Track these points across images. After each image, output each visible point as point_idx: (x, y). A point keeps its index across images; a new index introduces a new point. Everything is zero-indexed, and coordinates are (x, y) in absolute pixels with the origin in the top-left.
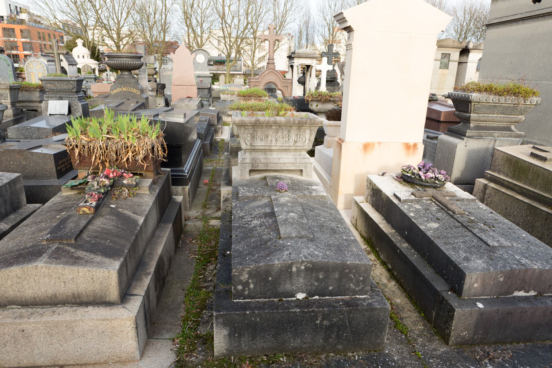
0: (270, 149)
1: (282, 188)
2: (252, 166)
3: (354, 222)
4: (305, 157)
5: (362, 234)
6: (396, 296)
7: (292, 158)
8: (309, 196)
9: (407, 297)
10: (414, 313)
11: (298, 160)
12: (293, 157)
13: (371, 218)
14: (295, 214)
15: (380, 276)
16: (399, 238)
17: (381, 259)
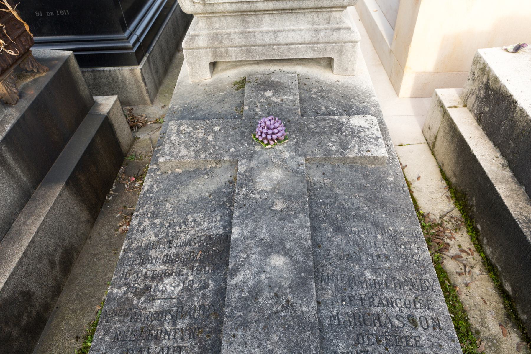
0: (253, 8)
1: (269, 137)
2: (215, 54)
4: (340, 26)
7: (309, 30)
8: (340, 159)
11: (322, 34)
12: (309, 26)
13: (474, 157)
14: (287, 260)
15: (483, 307)
17: (485, 253)
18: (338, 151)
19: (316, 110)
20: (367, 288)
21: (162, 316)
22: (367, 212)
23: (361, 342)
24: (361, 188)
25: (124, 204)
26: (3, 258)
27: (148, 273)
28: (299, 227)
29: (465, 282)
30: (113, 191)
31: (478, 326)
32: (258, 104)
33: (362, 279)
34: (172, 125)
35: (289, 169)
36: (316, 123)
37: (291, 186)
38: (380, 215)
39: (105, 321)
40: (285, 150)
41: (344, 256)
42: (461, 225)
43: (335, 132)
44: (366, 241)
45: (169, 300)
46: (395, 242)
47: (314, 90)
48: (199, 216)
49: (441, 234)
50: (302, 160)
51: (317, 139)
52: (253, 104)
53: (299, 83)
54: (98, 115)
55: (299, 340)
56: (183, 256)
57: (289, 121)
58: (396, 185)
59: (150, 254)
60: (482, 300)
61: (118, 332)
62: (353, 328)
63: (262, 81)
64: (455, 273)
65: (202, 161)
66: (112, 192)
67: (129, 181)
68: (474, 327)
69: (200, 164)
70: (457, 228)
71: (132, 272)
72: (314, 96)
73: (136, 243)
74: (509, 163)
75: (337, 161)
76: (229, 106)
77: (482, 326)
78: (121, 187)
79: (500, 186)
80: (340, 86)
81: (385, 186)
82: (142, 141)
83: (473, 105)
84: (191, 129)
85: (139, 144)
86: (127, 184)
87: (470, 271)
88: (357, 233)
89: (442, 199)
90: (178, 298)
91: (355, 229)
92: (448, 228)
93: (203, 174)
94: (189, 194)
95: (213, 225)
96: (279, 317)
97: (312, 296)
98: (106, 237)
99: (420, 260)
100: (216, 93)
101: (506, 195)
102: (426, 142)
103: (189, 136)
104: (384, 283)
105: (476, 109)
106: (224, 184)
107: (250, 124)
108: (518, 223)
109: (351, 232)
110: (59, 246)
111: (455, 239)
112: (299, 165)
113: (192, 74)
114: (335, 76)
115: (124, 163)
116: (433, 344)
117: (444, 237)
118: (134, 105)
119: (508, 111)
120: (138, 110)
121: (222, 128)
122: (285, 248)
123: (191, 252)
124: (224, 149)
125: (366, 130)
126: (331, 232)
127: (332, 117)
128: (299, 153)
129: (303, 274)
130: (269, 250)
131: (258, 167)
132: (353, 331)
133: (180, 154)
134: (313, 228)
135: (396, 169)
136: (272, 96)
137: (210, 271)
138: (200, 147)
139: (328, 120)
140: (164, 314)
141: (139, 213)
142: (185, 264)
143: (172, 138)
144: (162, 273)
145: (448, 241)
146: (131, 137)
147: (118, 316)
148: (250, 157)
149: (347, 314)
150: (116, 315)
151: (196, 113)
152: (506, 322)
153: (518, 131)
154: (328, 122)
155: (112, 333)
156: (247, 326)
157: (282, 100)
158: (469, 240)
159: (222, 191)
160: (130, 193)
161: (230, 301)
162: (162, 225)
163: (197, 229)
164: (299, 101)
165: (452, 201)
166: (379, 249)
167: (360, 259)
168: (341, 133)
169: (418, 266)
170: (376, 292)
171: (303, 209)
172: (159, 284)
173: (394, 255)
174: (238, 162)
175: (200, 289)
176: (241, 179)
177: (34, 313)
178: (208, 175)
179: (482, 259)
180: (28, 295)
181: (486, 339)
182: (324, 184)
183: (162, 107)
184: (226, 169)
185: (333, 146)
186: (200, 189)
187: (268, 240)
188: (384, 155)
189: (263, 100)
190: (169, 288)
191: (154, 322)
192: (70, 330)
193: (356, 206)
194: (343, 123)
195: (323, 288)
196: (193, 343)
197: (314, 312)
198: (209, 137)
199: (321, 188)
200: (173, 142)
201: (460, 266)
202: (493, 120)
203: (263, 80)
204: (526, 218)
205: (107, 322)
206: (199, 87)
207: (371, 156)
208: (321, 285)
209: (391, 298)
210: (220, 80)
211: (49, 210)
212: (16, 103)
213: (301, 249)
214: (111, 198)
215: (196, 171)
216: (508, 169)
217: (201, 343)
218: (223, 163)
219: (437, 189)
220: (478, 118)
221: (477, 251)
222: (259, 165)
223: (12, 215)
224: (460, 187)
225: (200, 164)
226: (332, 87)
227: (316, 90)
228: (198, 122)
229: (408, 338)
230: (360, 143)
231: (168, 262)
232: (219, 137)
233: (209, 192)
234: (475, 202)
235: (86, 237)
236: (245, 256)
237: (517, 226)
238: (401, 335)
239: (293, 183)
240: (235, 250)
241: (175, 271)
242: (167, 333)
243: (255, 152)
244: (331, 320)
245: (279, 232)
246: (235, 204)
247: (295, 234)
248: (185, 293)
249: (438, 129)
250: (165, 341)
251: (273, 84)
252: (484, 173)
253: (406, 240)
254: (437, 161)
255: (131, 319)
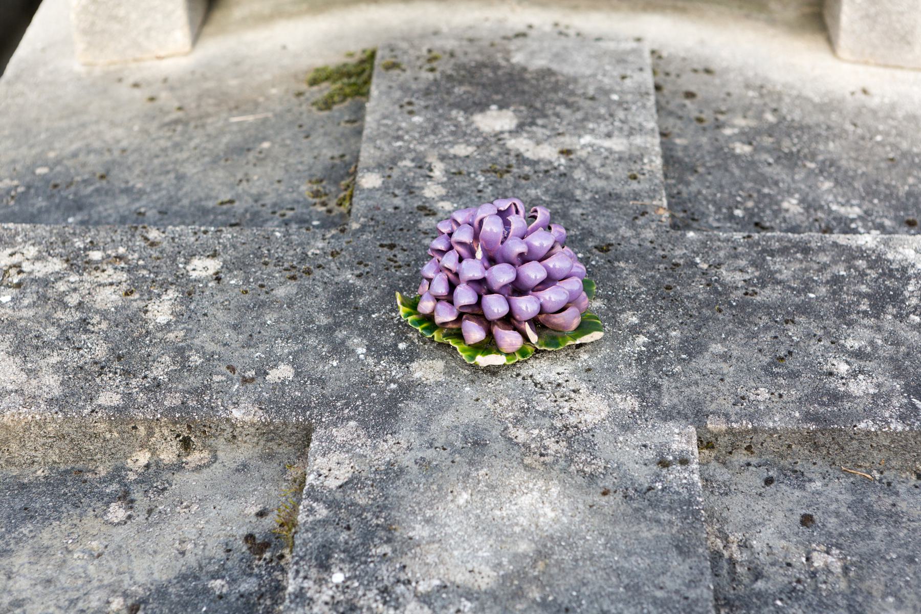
1: (496, 306)
18: (888, 400)
32: (438, 171)
35: (608, 483)
36: (753, 264)
37: (618, 572)
43: (863, 307)
47: (740, 122)
51: (768, 337)
52: (408, 163)
53: (658, 88)
63: (459, 67)
65: (102, 427)
72: (741, 149)
75: (885, 454)
76: (279, 174)
80: (874, 112)
84: (56, 265)
93: (101, 496)
100: (208, 115)
103: (44, 298)
106: (221, 554)
107: (390, 254)
112: (664, 464)
113: (93, 24)
114: (846, 67)
121: (228, 267)
124: (232, 369)
128: (666, 401)
131: (422, 463)
136: (514, 133)
139: (821, 249)
151: (92, 205)
154: (824, 258)
157: (566, 152)
159: (206, 591)
164: (658, 162)
176: (325, 522)
182: (813, 575)
184: (239, 477)
186: (76, 577)
189: (461, 150)
194: (904, 270)
203: (464, 60)
206: (124, 91)
210: (237, 64)
215: (64, 483)
218: (220, 443)
222: (429, 454)
226: (834, 116)
227: (752, 123)
228: (103, 235)
232: (212, 311)
233: (125, 595)
239: (630, 553)
243: (408, 390)
251: (523, 80)
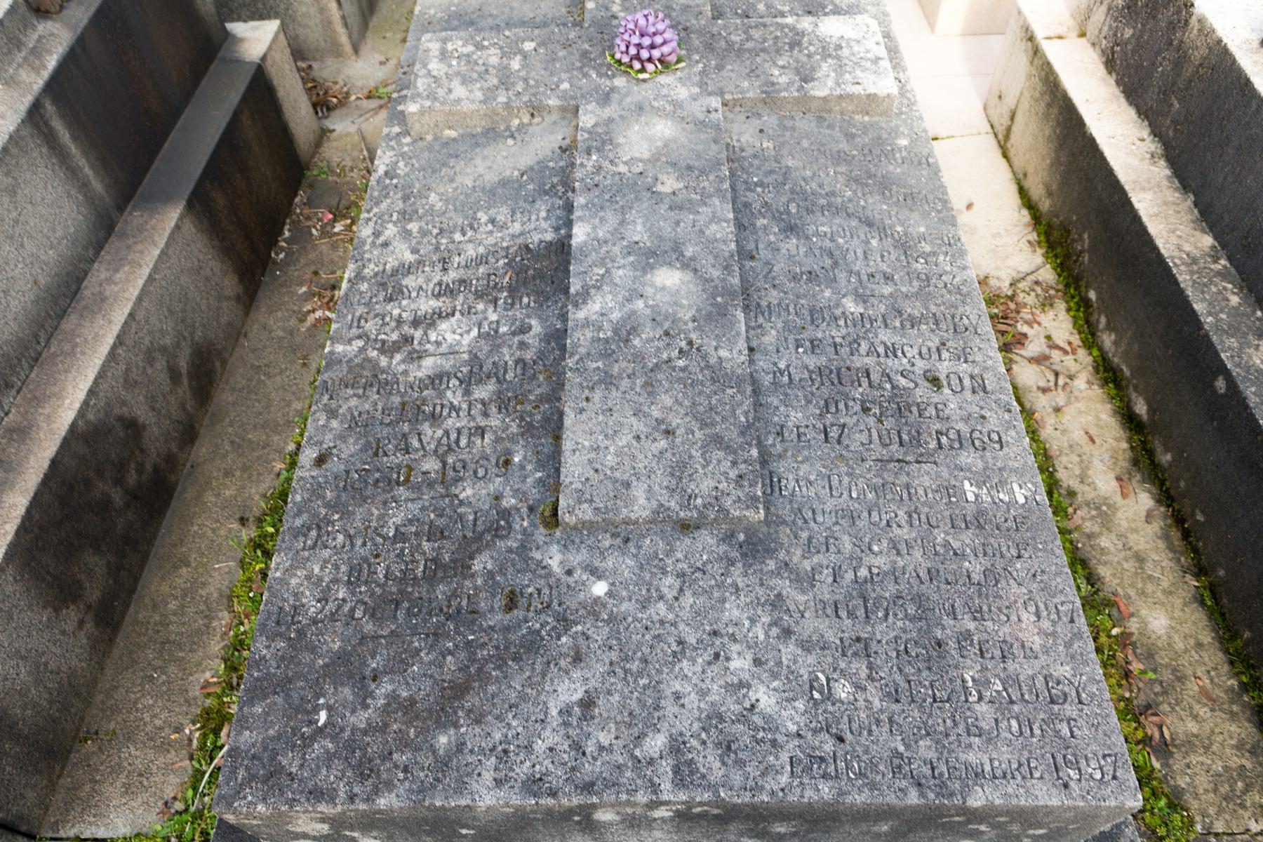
1: (645, 54)
3: (1002, 122)
5: (1026, 184)
6: (1150, 588)
8: (797, 101)
9: (1202, 603)
10: (1233, 716)
13: (1092, 142)
14: (689, 276)
15: (1087, 448)
16: (1235, 300)
17: (1100, 349)
19: (744, 11)
20: (846, 326)
21: (441, 381)
22: (850, 200)
23: (833, 410)
24: (839, 158)
25: (313, 268)
26: (76, 345)
27: (404, 315)
28: (711, 222)
29: (1054, 404)
30: (285, 240)
31: (1074, 484)
33: (838, 312)
34: (430, 41)
36: (744, 33)
38: (876, 206)
39: (326, 397)
40: (679, 85)
41: (802, 273)
42: (1055, 297)
44: (847, 250)
45: (452, 356)
46: (905, 253)
48: (502, 214)
49: (1010, 315)
50: (715, 102)
54: (239, 62)
55: (714, 402)
56: (474, 282)
57: (685, 29)
58: (912, 154)
59: (404, 283)
60: (1086, 436)
61: (356, 414)
62: (818, 389)
64: (1035, 389)
65: (501, 110)
66: (284, 244)
67: (320, 220)
68: (1065, 485)
69: (496, 118)
70: (1047, 303)
71: (372, 315)
73: (372, 266)
74: (1166, 149)
77: (1082, 482)
78: (302, 235)
79: (1142, 195)
81: (889, 155)
82: (341, 136)
83: (1100, 30)
84: (470, 48)
85: (334, 144)
86: (315, 227)
87: (1066, 384)
88: (829, 236)
89: (1018, 248)
90: (470, 352)
91: (824, 229)
92: (1025, 305)
94: (476, 175)
95: (533, 226)
96: (674, 369)
97: (738, 334)
98: (281, 334)
99: (954, 282)
101: (1151, 212)
102: (991, 130)
104: (880, 319)
105: (1105, 38)
106: (551, 154)
108: (1171, 264)
109: (817, 234)
110: (185, 338)
111: (1039, 324)
112: (709, 112)
115: (305, 182)
116: (970, 415)
117: (1017, 322)
118: (315, 59)
119: (1174, 28)
120: (325, 70)
121: (539, 45)
122: (683, 256)
123: (489, 275)
125: (853, 44)
126: (775, 234)
127: (779, 20)
129: (719, 299)
130: (652, 261)
131: (621, 117)
132: (818, 393)
133: (452, 97)
134: (740, 226)
135: (915, 124)
137: (532, 304)
138: (495, 81)
140: (445, 379)
141: (371, 215)
142: (479, 295)
143: (431, 66)
144: (434, 313)
145: (1024, 329)
146: (315, 125)
147: (353, 387)
148: (605, 98)
149: (807, 367)
150: (347, 387)
152: (1130, 474)
153: (1190, 70)
155: (344, 414)
156: (611, 383)
158: (1070, 326)
159: (547, 167)
160: (324, 245)
161: (576, 345)
162: (424, 233)
163: (499, 235)
165: (1040, 251)
166: (872, 263)
167: (835, 280)
168: (800, 51)
169: (949, 292)
170: (865, 333)
171: (719, 190)
172: (429, 332)
173: (902, 274)
174: (578, 110)
175: (514, 334)
176: (588, 139)
177: (149, 468)
178: (515, 138)
179: (1095, 361)
180: (133, 427)
181: (1088, 504)
183: (381, 63)
185: (781, 75)
187: (648, 244)
188: (890, 91)
190: (450, 337)
191: (426, 393)
192: (227, 507)
193: (827, 189)
195: (760, 326)
196: (507, 420)
197: (743, 358)
198: (512, 63)
199: (755, 156)
200: (433, 74)
201: (1047, 375)
202: (1140, 56)
204: (1188, 255)
205: (331, 398)
207: (862, 92)
208: (756, 321)
209: (893, 344)
211: (159, 256)
212: (60, 11)
213: (715, 257)
214: (282, 256)
216: (1162, 163)
217: (522, 419)
219: (1009, 228)
220: (1108, 58)
221: (1085, 346)
222: (623, 113)
223: (80, 261)
224: (1058, 218)
225: (496, 118)
228: (487, 35)
229: (923, 406)
230: (840, 68)
231: (445, 294)
234: (1087, 241)
235: (236, 333)
236: (602, 271)
237: (1167, 270)
238: (910, 400)
240: (581, 261)
241: (459, 308)
242: (454, 409)
243: (613, 89)
244: (774, 377)
245: (669, 230)
246: (577, 184)
247: (702, 232)
248: (483, 342)
249: (1018, 94)
250: (450, 422)
252: (1110, 173)
253: (928, 249)
254: (1013, 171)
255: (379, 390)
